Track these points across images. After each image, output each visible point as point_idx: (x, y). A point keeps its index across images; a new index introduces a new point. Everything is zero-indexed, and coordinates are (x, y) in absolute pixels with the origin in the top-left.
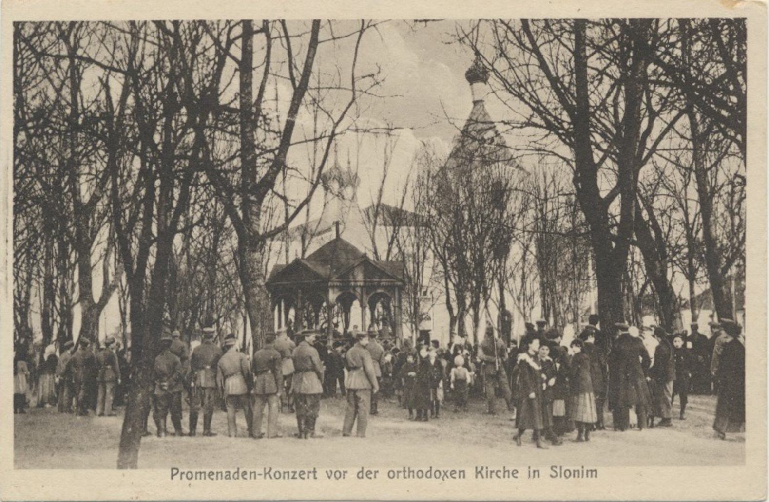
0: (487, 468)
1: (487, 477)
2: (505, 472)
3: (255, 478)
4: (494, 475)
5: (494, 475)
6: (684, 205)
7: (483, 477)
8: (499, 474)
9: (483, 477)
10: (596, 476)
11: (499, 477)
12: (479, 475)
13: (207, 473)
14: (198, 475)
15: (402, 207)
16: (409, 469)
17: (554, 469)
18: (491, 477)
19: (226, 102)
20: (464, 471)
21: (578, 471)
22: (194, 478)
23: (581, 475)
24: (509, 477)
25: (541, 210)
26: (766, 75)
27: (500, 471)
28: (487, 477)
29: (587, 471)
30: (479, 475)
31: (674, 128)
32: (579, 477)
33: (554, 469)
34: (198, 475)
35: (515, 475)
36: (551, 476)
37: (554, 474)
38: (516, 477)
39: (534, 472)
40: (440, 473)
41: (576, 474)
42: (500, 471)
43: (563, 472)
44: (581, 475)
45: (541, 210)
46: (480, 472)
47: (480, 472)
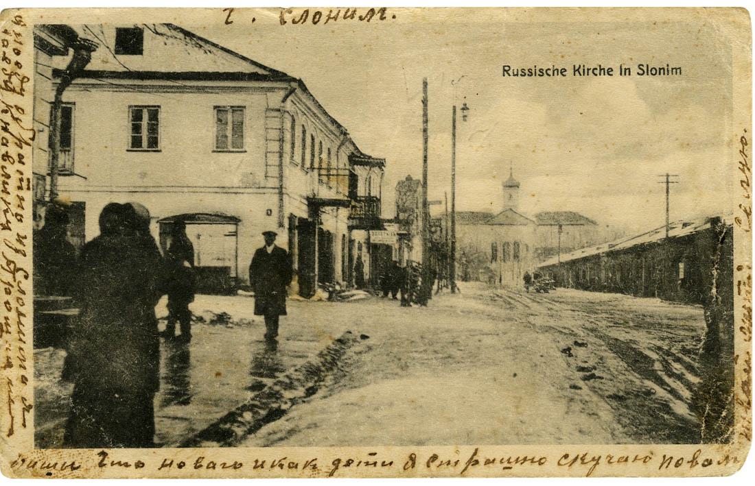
0: (584, 66)
1: (584, 75)
2: (601, 70)
3: (629, 74)
4: (590, 72)
5: (590, 72)
6: (261, 71)
7: (580, 75)
8: (595, 71)
9: (580, 75)
10: (629, 74)
11: (596, 75)
12: (577, 73)
13: (560, 70)
14: (674, 70)
15: (369, 194)
16: (600, 66)
17: (641, 67)
18: (588, 75)
19: (458, 285)
20: (629, 69)
21: (663, 69)
22: (646, 73)
23: (666, 72)
24: (604, 74)
25: (676, 327)
26: (751, 241)
27: (596, 69)
28: (584, 75)
29: (672, 69)
30: (577, 73)
31: (667, 236)
32: (664, 74)
33: (641, 67)
34: (674, 70)
35: (610, 73)
36: (638, 74)
37: (641, 72)
38: (612, 75)
39: (625, 69)
40: (656, 70)
41: (662, 71)
42: (596, 69)
43: (649, 70)
44: (666, 72)
45: (676, 327)
46: (578, 70)
47: (578, 70)
